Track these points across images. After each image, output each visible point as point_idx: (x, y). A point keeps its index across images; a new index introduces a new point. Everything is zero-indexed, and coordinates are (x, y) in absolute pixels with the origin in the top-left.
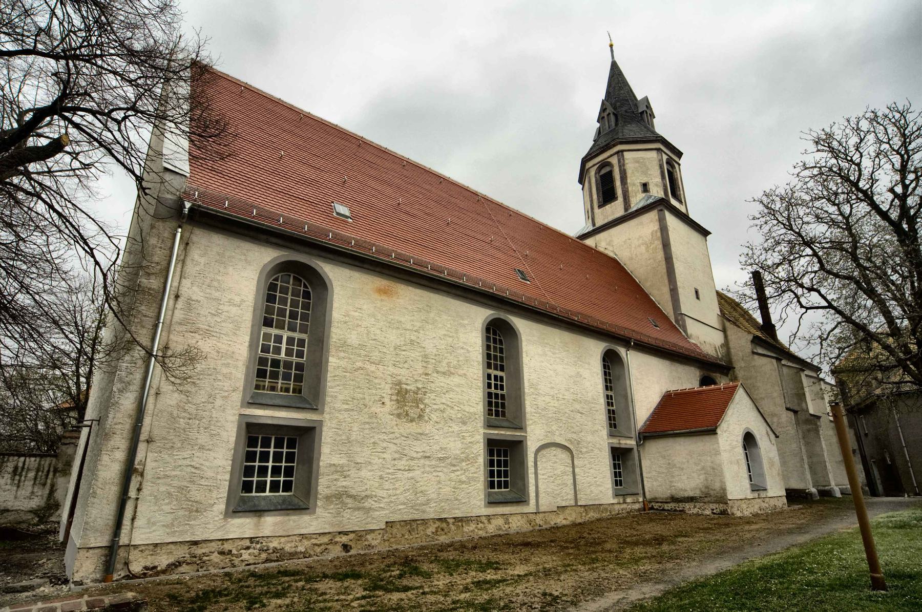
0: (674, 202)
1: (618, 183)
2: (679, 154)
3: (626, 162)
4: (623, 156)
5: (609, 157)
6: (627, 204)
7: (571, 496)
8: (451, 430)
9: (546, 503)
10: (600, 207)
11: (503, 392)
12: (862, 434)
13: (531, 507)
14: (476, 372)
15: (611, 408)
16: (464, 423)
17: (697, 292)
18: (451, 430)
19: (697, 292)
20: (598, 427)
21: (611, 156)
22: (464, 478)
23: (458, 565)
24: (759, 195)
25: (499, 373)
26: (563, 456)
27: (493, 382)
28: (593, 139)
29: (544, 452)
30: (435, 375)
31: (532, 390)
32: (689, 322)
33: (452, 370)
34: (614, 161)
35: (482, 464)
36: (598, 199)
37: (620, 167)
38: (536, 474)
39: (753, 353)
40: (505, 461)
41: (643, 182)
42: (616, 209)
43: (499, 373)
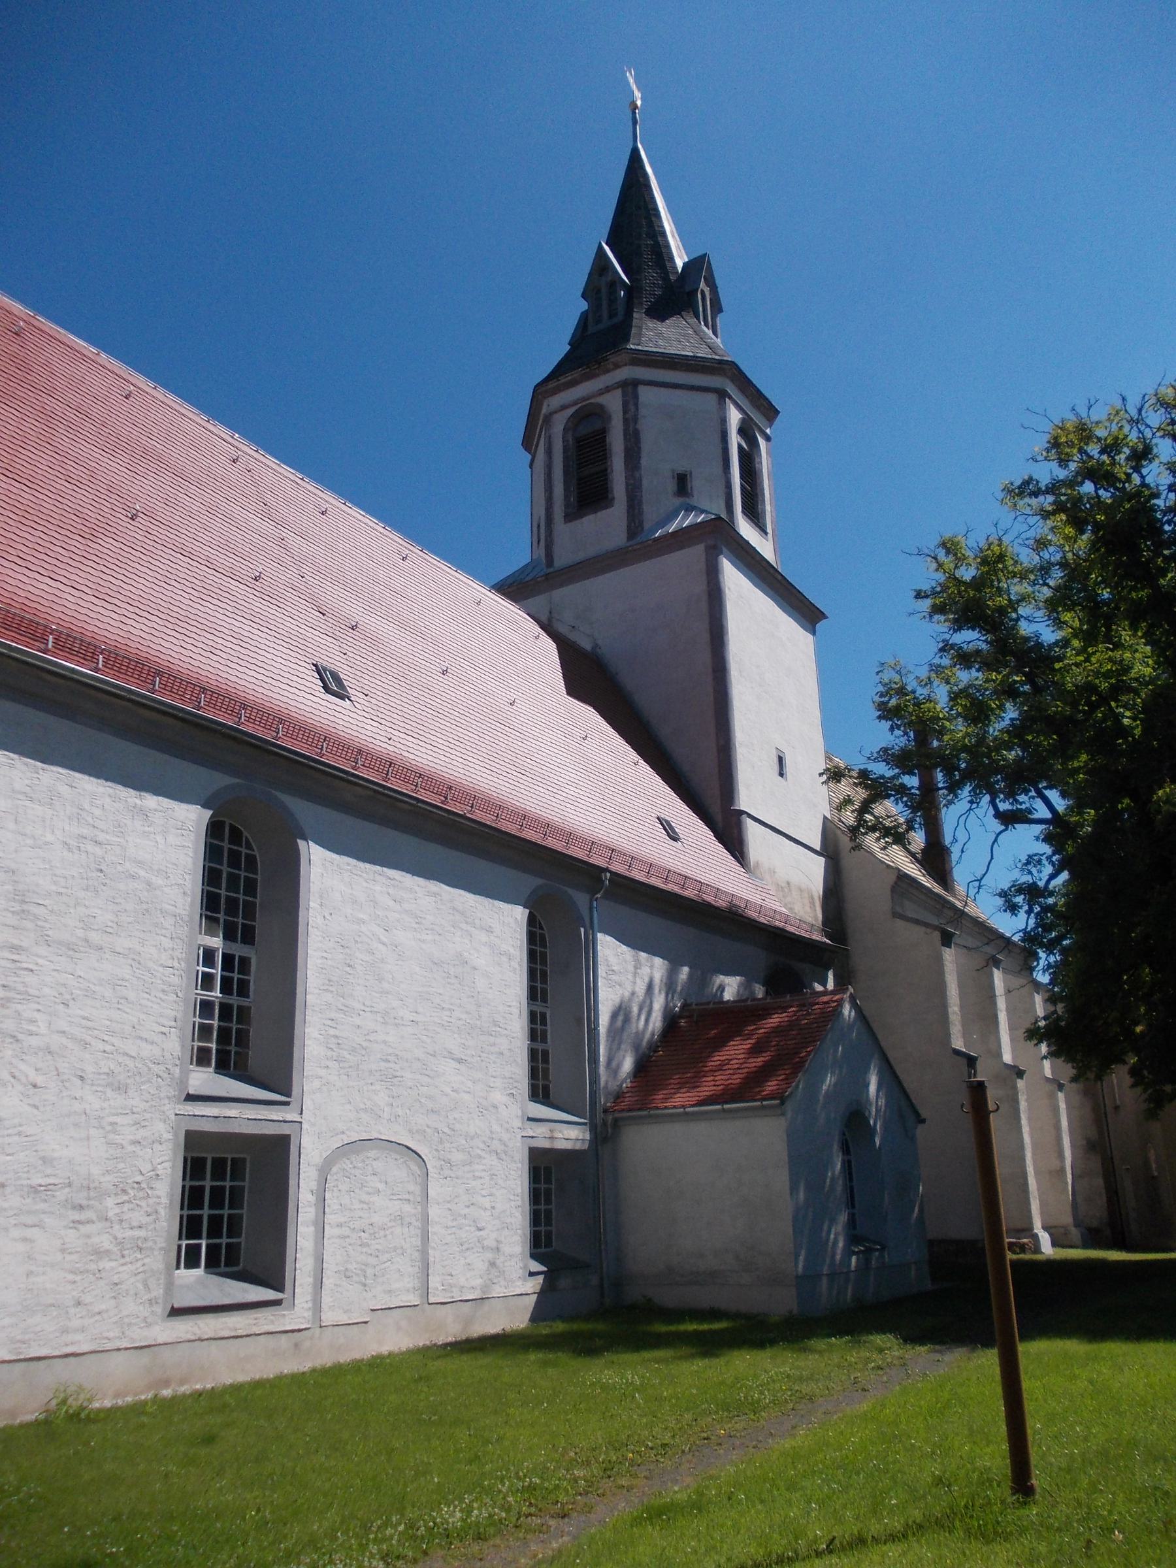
0: (745, 529)
1: (617, 464)
2: (771, 412)
3: (643, 411)
4: (636, 397)
5: (601, 392)
6: (635, 524)
7: (410, 1282)
8: (77, 1106)
9: (343, 1301)
10: (569, 517)
11: (244, 1002)
12: (1109, 1110)
13: (297, 1314)
14: (167, 943)
15: (540, 1047)
16: (122, 1089)
17: (780, 759)
18: (77, 1106)
19: (780, 759)
20: (498, 1097)
21: (608, 389)
22: (106, 1242)
23: (159, 871)
24: (931, 543)
25: (239, 950)
26: (398, 1171)
27: (217, 971)
28: (568, 337)
29: (346, 1164)
30: (42, 950)
31: (328, 997)
32: (749, 822)
33: (95, 937)
34: (613, 403)
35: (165, 1201)
36: (566, 497)
37: (626, 421)
38: (322, 1201)
39: (896, 915)
40: (232, 1208)
41: (681, 470)
42: (606, 528)
43: (239, 950)
